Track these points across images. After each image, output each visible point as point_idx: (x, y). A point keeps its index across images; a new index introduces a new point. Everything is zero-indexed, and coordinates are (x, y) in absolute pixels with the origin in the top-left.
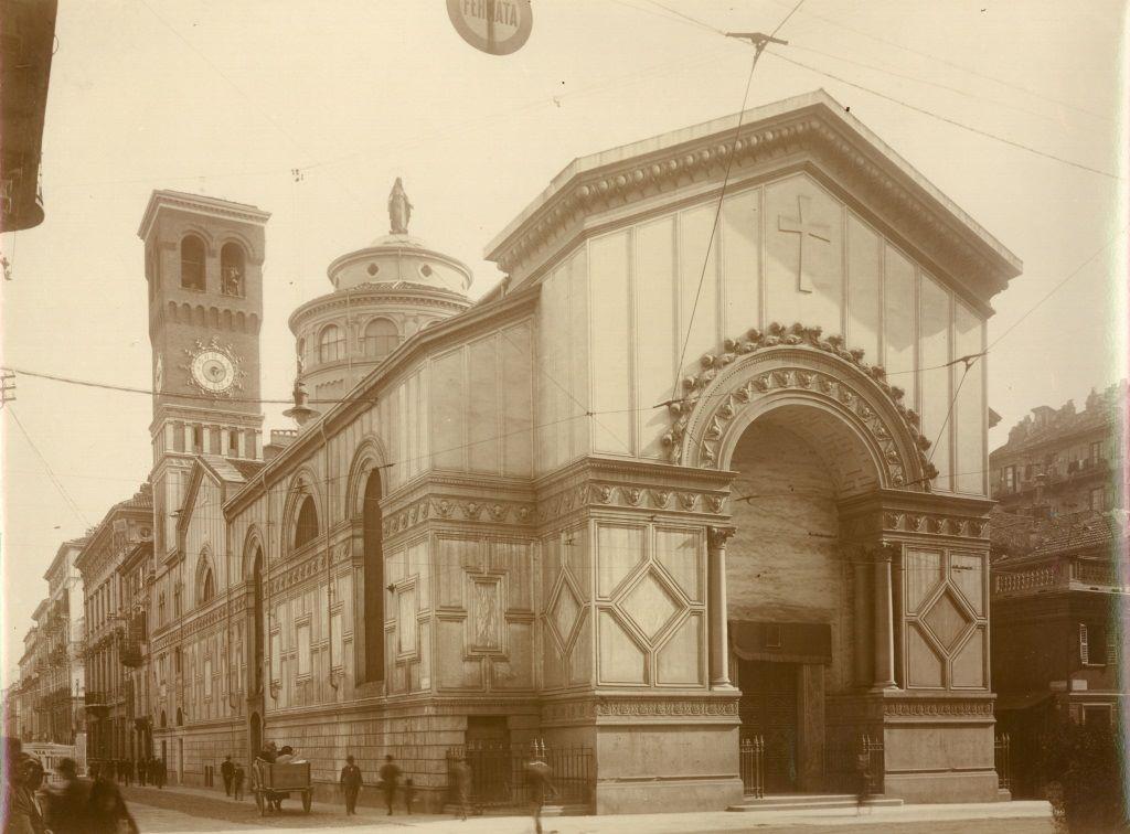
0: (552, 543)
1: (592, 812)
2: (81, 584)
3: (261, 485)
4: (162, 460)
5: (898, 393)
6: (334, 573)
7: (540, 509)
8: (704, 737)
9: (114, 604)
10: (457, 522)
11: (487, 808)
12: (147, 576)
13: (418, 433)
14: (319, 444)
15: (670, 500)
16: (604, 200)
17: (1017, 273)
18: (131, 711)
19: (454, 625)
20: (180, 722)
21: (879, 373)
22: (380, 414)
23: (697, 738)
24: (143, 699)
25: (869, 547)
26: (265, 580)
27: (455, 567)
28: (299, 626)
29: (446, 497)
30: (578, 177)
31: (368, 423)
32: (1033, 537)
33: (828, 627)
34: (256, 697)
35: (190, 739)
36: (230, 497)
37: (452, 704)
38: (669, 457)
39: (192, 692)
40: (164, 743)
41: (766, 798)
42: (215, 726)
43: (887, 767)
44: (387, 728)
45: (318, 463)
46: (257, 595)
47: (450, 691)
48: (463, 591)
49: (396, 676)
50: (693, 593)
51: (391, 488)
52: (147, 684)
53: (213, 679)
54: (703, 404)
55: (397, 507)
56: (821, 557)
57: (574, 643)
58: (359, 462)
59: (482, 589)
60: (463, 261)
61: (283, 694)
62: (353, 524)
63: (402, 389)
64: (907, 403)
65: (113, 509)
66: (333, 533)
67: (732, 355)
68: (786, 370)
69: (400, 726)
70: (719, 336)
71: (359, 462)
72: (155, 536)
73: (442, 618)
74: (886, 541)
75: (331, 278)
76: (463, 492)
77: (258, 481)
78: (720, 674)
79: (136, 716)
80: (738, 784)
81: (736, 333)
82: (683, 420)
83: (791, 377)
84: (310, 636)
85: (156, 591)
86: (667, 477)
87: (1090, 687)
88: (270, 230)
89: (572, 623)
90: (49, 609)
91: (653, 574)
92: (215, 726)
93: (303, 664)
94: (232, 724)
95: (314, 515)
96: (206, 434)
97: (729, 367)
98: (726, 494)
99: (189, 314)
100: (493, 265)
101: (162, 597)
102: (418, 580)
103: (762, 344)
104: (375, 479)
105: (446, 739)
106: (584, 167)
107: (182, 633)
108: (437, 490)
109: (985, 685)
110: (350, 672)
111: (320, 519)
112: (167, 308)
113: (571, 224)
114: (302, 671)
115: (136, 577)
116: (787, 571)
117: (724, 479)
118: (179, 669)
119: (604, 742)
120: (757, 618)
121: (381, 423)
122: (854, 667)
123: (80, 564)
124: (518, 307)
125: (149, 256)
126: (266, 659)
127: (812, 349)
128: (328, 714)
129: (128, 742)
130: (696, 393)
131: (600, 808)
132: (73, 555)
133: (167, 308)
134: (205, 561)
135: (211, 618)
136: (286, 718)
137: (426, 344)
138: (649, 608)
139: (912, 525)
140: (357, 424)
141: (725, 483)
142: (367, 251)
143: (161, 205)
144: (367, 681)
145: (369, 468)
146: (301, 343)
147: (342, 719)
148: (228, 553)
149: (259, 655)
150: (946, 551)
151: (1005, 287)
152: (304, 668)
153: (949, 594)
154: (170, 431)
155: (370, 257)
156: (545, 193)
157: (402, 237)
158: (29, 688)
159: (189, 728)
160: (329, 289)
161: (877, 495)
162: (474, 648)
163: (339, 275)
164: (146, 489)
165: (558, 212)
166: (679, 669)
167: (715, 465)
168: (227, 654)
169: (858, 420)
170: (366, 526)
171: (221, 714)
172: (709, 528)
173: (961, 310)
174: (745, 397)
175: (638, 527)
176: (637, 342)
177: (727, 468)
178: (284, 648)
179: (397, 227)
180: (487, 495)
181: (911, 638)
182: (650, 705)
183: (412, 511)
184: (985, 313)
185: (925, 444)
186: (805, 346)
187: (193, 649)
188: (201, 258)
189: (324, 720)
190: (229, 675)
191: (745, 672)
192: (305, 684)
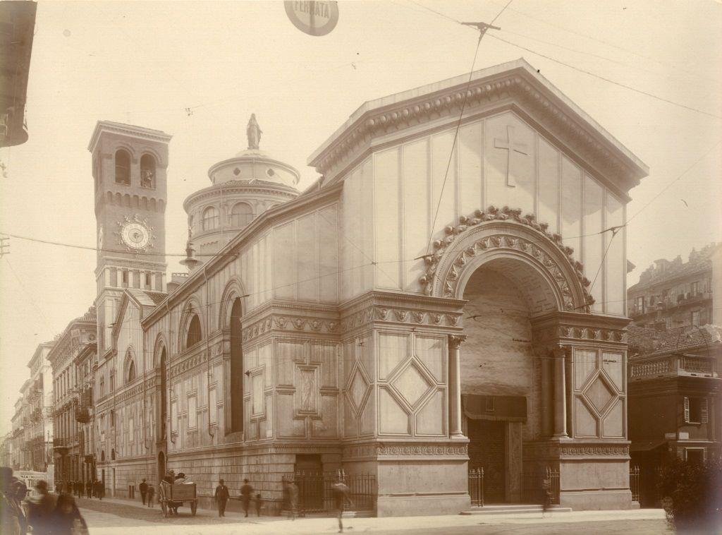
2: (51, 370)
4: (103, 291)
5: (569, 251)
9: (72, 383)
10: (290, 331)
12: (93, 365)
15: (425, 318)
17: (645, 175)
20: (114, 458)
21: (558, 238)
24: (90, 443)
25: (551, 348)
28: (189, 397)
29: (283, 316)
34: (162, 442)
35: (120, 468)
37: (286, 447)
38: (424, 291)
39: (121, 438)
40: (103, 471)
41: (485, 507)
43: (562, 488)
44: (245, 461)
45: (202, 294)
48: (293, 375)
49: (250, 429)
52: (93, 433)
53: (135, 430)
55: (251, 322)
56: (521, 354)
57: (363, 407)
61: (179, 440)
62: (224, 332)
63: (255, 247)
64: (576, 257)
66: (210, 338)
67: (465, 226)
68: (498, 236)
69: (253, 460)
70: (456, 214)
71: (228, 292)
74: (561, 344)
76: (294, 313)
78: (456, 428)
79: (86, 454)
80: (467, 498)
82: (433, 267)
83: (502, 240)
84: (196, 403)
85: (99, 374)
86: (423, 303)
90: (30, 386)
91: (414, 365)
95: (198, 322)
96: (131, 276)
97: (462, 234)
98: (461, 314)
101: (102, 378)
102: (265, 368)
103: (484, 220)
104: (237, 303)
105: (283, 469)
106: (372, 107)
107: (115, 402)
108: (277, 311)
109: (624, 435)
110: (222, 426)
113: (362, 143)
114: (191, 425)
115: (86, 365)
116: (497, 362)
117: (458, 305)
118: (113, 424)
119: (382, 472)
120: (480, 393)
122: (541, 424)
123: (51, 357)
124: (328, 195)
127: (515, 222)
128: (207, 452)
130: (441, 251)
131: (379, 513)
132: (46, 352)
134: (130, 356)
135: (133, 392)
138: (411, 386)
139: (578, 334)
140: (226, 269)
143: (103, 130)
145: (234, 297)
146: (191, 219)
147: (216, 456)
149: (164, 415)
150: (600, 350)
151: (638, 183)
152: (192, 424)
153: (601, 377)
154: (108, 272)
155: (235, 164)
157: (255, 151)
159: (119, 462)
160: (208, 184)
161: (556, 315)
162: (300, 411)
164: (92, 310)
168: (143, 415)
171: (140, 453)
172: (449, 336)
173: (611, 199)
174: (473, 253)
175: (404, 335)
176: (408, 218)
177: (461, 298)
179: (252, 144)
180: (309, 314)
181: (577, 406)
183: (261, 325)
185: (586, 283)
186: (511, 221)
187: (122, 412)
188: (128, 165)
189: (205, 457)
190: (145, 428)
192: (193, 433)
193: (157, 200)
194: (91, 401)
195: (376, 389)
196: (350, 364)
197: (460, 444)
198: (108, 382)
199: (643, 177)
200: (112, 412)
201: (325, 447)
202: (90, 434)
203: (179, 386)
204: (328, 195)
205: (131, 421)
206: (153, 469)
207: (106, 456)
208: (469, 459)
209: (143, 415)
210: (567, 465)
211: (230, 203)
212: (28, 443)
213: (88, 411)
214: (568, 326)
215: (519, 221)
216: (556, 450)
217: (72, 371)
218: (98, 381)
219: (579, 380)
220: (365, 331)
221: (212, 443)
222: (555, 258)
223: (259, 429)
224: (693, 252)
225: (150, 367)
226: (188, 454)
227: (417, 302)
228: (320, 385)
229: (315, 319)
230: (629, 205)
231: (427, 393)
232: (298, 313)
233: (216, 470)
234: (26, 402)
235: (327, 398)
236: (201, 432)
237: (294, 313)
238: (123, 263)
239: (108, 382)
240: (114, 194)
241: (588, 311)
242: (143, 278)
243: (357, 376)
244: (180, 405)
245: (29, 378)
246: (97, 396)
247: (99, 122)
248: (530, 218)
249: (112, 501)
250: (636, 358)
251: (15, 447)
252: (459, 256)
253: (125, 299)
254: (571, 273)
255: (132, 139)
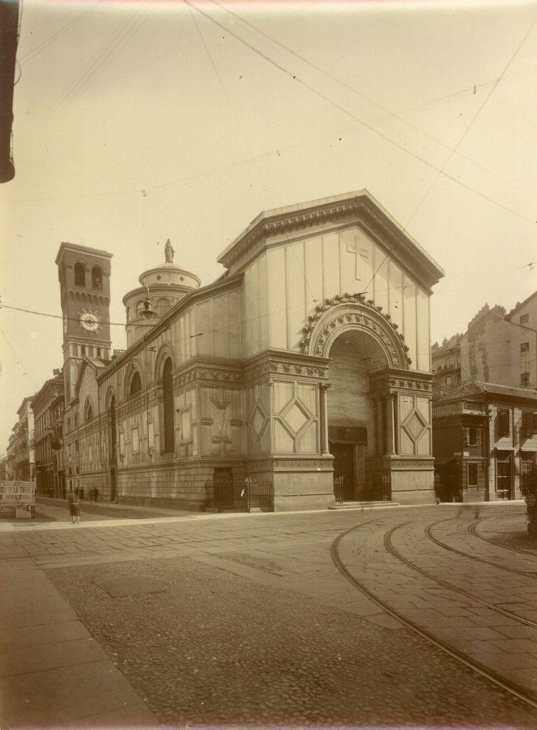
0: (251, 390)
1: (272, 511)
2: (33, 415)
3: (114, 368)
4: (67, 362)
5: (396, 327)
7: (245, 375)
8: (409, 475)
9: (48, 422)
10: (209, 380)
12: (62, 410)
13: (189, 339)
15: (304, 371)
17: (442, 276)
18: (55, 469)
19: (208, 427)
20: (78, 473)
21: (388, 317)
22: (171, 333)
24: (61, 463)
25: (384, 394)
27: (208, 400)
28: (132, 429)
29: (204, 368)
30: (264, 220)
31: (165, 337)
34: (113, 461)
36: (99, 375)
38: (303, 351)
39: (83, 459)
40: (71, 482)
42: (94, 474)
43: (393, 489)
44: (176, 473)
45: (141, 356)
46: (112, 417)
47: (206, 456)
48: (212, 412)
49: (180, 451)
53: (93, 454)
57: (262, 434)
58: (161, 354)
59: (220, 411)
60: (196, 274)
61: (125, 460)
62: (159, 383)
63: (182, 320)
64: (399, 331)
65: (47, 382)
66: (149, 387)
67: (329, 306)
68: (351, 314)
69: (183, 472)
70: (323, 297)
71: (161, 354)
72: (65, 393)
74: (392, 391)
79: (59, 470)
80: (333, 497)
81: (330, 297)
82: (309, 334)
83: (353, 317)
84: (139, 435)
85: (66, 416)
86: (302, 360)
88: (113, 261)
89: (261, 426)
91: (297, 404)
92: (94, 474)
94: (102, 473)
95: (139, 379)
96: (87, 349)
97: (328, 311)
100: (221, 265)
101: (69, 419)
103: (341, 302)
104: (169, 363)
105: (205, 478)
106: (266, 216)
108: (200, 365)
109: (430, 454)
110: (158, 449)
111: (142, 381)
113: (259, 243)
114: (135, 449)
115: (57, 411)
116: (351, 405)
117: (325, 362)
118: (77, 449)
119: (277, 478)
120: (337, 425)
121: (171, 336)
122: (377, 446)
123: (32, 407)
126: (117, 444)
128: (147, 468)
130: (314, 323)
132: (29, 403)
134: (88, 403)
135: (91, 427)
136: (127, 470)
137: (194, 298)
138: (295, 419)
139: (402, 384)
140: (160, 337)
141: (326, 363)
145: (166, 357)
146: (128, 309)
147: (155, 469)
148: (99, 398)
152: (135, 448)
153: (416, 414)
154: (71, 347)
156: (247, 229)
159: (82, 475)
160: (139, 286)
161: (388, 371)
162: (217, 437)
163: (144, 280)
165: (253, 237)
166: (308, 447)
167: (322, 355)
168: (99, 443)
169: (373, 331)
172: (320, 384)
174: (334, 325)
175: (290, 382)
177: (327, 357)
179: (168, 259)
181: (402, 434)
182: (298, 462)
184: (430, 293)
186: (358, 304)
187: (83, 441)
188: (82, 274)
189: (145, 470)
191: (333, 448)
192: (136, 455)
193: (104, 298)
194: (61, 434)
197: (329, 460)
198: (73, 423)
200: (76, 442)
203: (125, 422)
204: (232, 283)
205: (90, 448)
207: (72, 471)
210: (396, 473)
211: (155, 298)
214: (395, 379)
217: (48, 415)
218: (66, 422)
219: (402, 416)
223: (187, 450)
224: (445, 340)
225: (103, 410)
226: (131, 469)
227: (298, 359)
228: (230, 418)
230: (432, 296)
232: (214, 367)
233: (154, 480)
234: (16, 437)
236: (142, 454)
238: (81, 341)
239: (73, 423)
241: (408, 369)
243: (257, 412)
244: (126, 435)
245: (18, 421)
246: (65, 431)
248: (371, 302)
250: (436, 403)
253: (85, 364)
255: (89, 256)
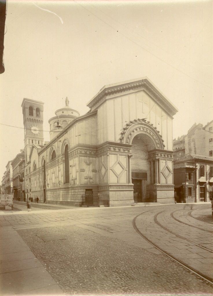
0: (100, 158)
2: (12, 168)
5: (159, 132)
6: (59, 164)
7: (98, 151)
11: (90, 206)
12: (24, 166)
13: (77, 137)
14: (56, 141)
16: (109, 94)
18: (21, 189)
19: (83, 173)
23: (126, 193)
24: (24, 187)
25: (154, 159)
26: (46, 165)
30: (105, 89)
31: (66, 136)
32: (177, 158)
33: (147, 173)
34: (45, 186)
35: (32, 194)
36: (39, 151)
37: (83, 187)
39: (32, 186)
40: (28, 195)
41: (138, 203)
42: (36, 192)
43: (157, 198)
45: (56, 144)
47: (82, 184)
48: (85, 166)
49: (71, 182)
50: (125, 167)
51: (70, 148)
52: (24, 185)
54: (127, 132)
55: (71, 151)
56: (146, 161)
61: (49, 186)
62: (63, 155)
64: (160, 134)
66: (59, 156)
67: (132, 124)
68: (140, 127)
69: (73, 191)
73: (81, 171)
74: (157, 158)
75: (56, 114)
76: (84, 148)
77: (44, 148)
78: (130, 181)
79: (22, 190)
80: (133, 201)
81: (132, 120)
84: (55, 175)
85: (26, 168)
87: (189, 184)
88: (44, 105)
90: (7, 172)
91: (119, 163)
92: (36, 192)
93: (54, 181)
94: (40, 191)
96: (34, 141)
98: (131, 149)
99: (31, 120)
100: (88, 107)
101: (27, 169)
102: (76, 164)
103: (137, 122)
104: (67, 146)
105: (82, 193)
106: (106, 87)
107: (31, 176)
108: (79, 148)
110: (63, 181)
112: (26, 119)
116: (141, 164)
117: (130, 146)
118: (30, 182)
119: (111, 193)
120: (135, 172)
121: (68, 136)
122: (151, 180)
123: (12, 164)
125: (23, 110)
127: (145, 123)
128: (58, 189)
129: (21, 195)
130: (126, 130)
131: (110, 206)
132: (11, 163)
133: (26, 119)
138: (118, 169)
140: (63, 136)
141: (131, 147)
142: (62, 109)
143: (25, 100)
144: (66, 183)
145: (66, 144)
147: (61, 190)
149: (45, 179)
150: (167, 160)
151: (175, 114)
152: (54, 181)
153: (167, 167)
154: (27, 140)
155: (62, 110)
156: (99, 93)
157: (68, 107)
158: (3, 186)
159: (32, 192)
160: (55, 116)
161: (155, 150)
163: (57, 113)
168: (39, 179)
170: (65, 155)
171: (38, 190)
173: (169, 118)
174: (134, 131)
177: (131, 144)
178: (50, 177)
180: (88, 149)
182: (120, 187)
183: (75, 152)
185: (163, 141)
186: (143, 123)
187: (33, 178)
190: (39, 183)
195: (109, 170)
196: (100, 163)
199: (177, 112)
200: (30, 179)
201: (93, 187)
202: (23, 185)
206: (42, 194)
208: (174, 185)
209: (39, 179)
210: (159, 191)
212: (6, 188)
213: (23, 179)
215: (146, 123)
216: (156, 187)
218: (25, 170)
220: (105, 153)
221: (60, 186)
222: (155, 133)
224: (179, 137)
225: (40, 166)
226: (52, 190)
227: (119, 145)
228: (92, 169)
229: (90, 150)
231: (123, 171)
232: (86, 148)
235: (94, 173)
237: (84, 148)
240: (29, 118)
242: (37, 142)
244: (50, 176)
246: (25, 174)
247: (24, 98)
249: (41, 204)
250: (175, 163)
251: (2, 189)
252: (130, 132)
253: (33, 147)
254: (159, 138)
255: (34, 103)
